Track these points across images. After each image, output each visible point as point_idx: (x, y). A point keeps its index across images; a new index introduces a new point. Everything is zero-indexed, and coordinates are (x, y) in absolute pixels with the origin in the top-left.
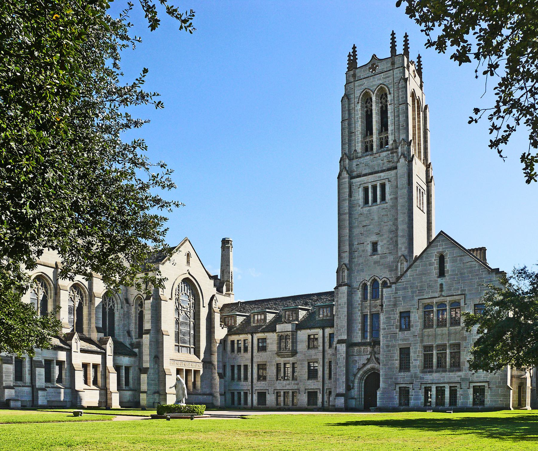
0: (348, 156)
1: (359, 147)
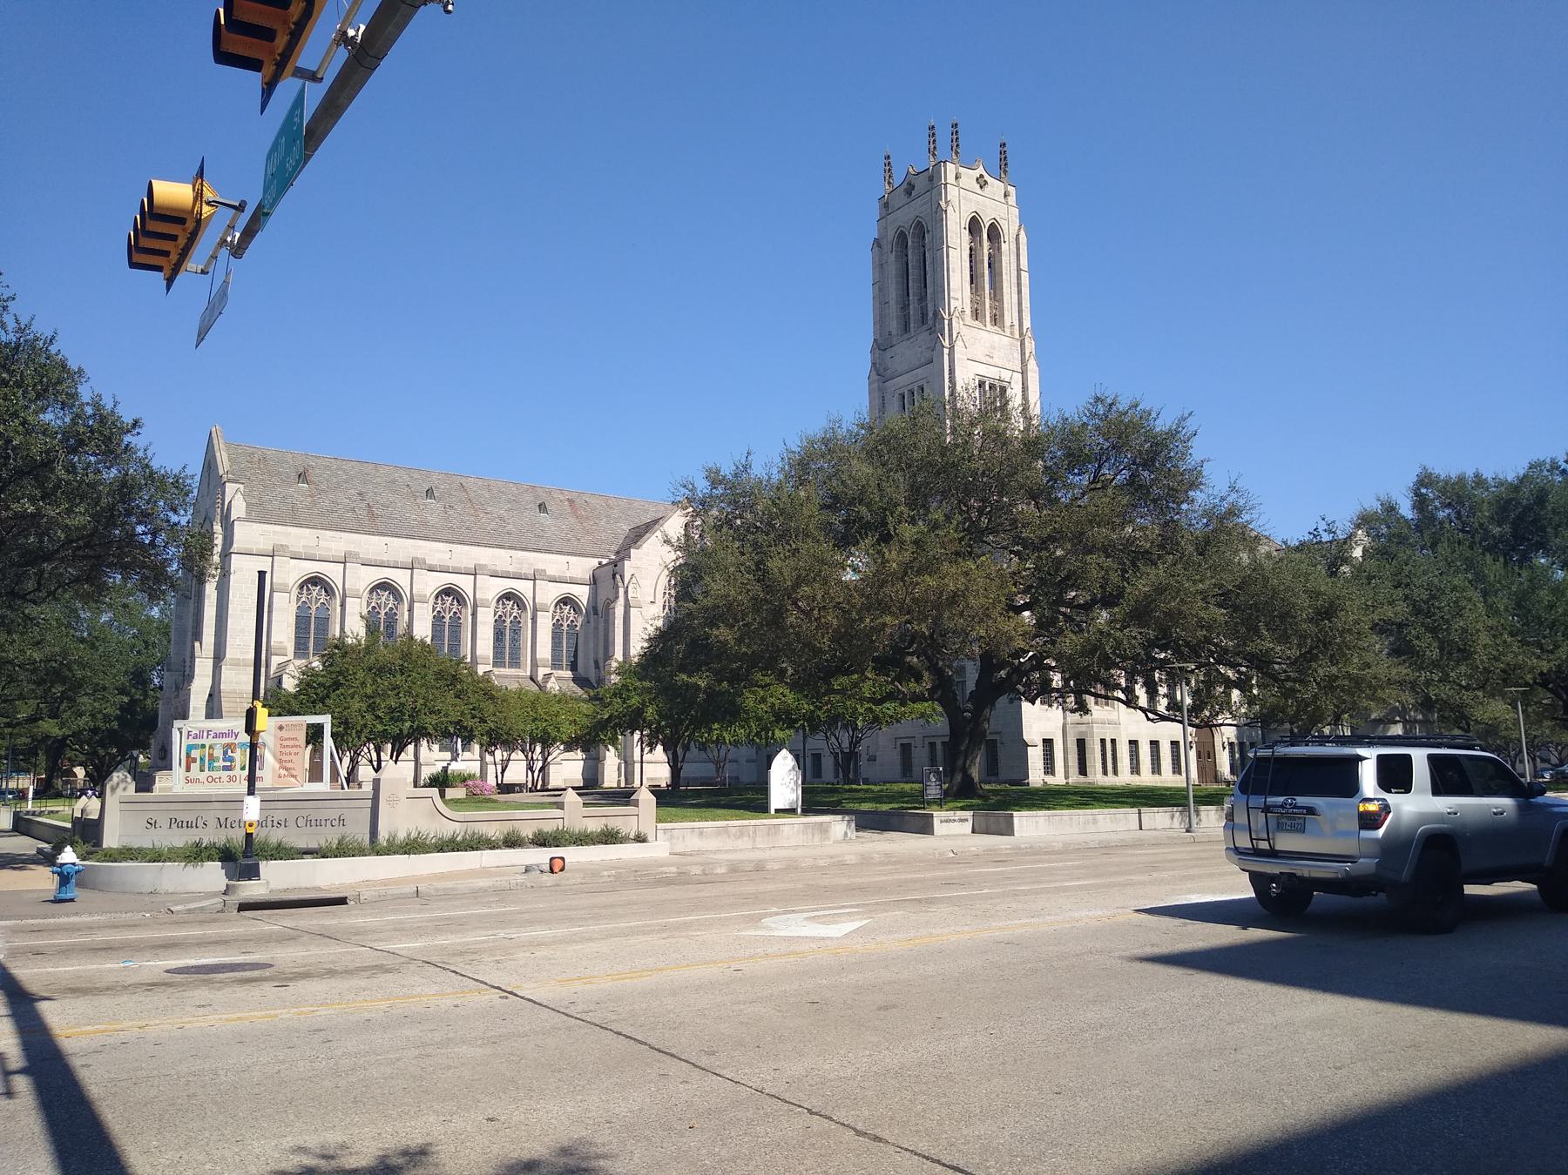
0: (882, 346)
1: (894, 325)
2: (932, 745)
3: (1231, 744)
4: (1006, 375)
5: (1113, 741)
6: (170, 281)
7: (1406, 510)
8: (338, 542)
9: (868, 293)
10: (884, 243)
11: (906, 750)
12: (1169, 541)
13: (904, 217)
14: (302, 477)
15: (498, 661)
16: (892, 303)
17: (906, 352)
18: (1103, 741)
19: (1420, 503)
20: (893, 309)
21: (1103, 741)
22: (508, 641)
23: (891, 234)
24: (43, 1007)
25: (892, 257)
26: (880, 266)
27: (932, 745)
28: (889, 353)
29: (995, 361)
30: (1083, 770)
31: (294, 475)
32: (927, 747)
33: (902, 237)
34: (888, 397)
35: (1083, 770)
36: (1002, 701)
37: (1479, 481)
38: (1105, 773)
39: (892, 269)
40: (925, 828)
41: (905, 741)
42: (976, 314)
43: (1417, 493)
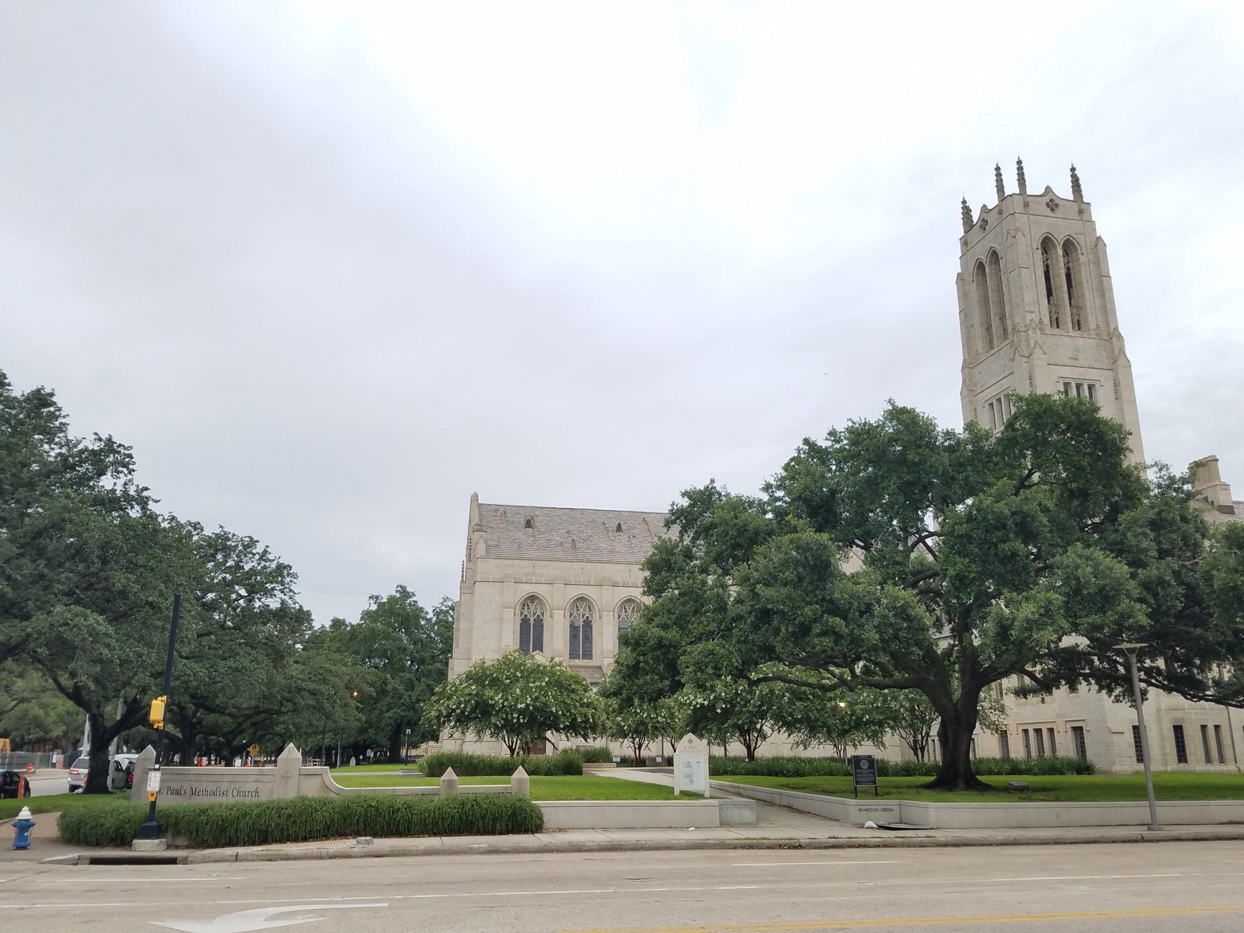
0: (969, 366)
1: (980, 345)
2: (1026, 731)
4: (1092, 375)
5: (1051, 730)
6: (967, 211)
8: (594, 570)
9: (1113, 272)
13: (982, 254)
14: (529, 524)
15: (574, 655)
16: (977, 325)
18: (1204, 727)
20: (978, 332)
22: (581, 637)
25: (973, 287)
28: (977, 370)
29: (1082, 362)
30: (1182, 756)
31: (523, 522)
33: (981, 266)
34: (979, 408)
35: (1182, 756)
38: (1208, 760)
39: (975, 296)
40: (229, 763)
42: (1056, 323)
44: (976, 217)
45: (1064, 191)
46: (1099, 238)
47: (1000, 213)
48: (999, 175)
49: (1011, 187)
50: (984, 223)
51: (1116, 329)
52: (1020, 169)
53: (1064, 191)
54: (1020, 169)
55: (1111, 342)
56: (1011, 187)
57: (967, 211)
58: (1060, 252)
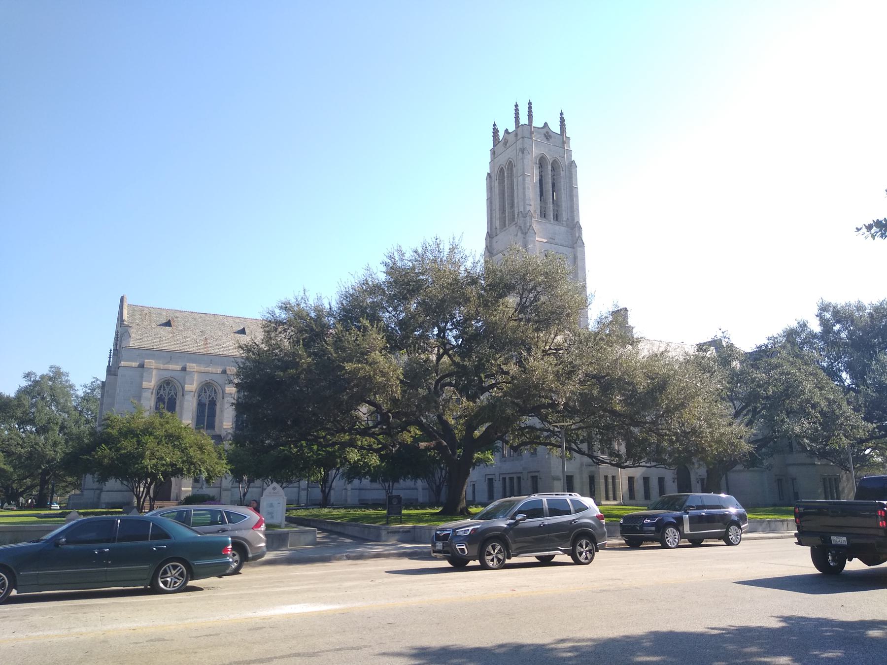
0: (490, 236)
1: (497, 223)
2: (504, 479)
3: (702, 480)
7: (816, 327)
10: (492, 175)
11: (491, 481)
12: (346, 372)
13: (502, 160)
14: (168, 324)
17: (505, 238)
18: (606, 477)
19: (824, 323)
20: (497, 214)
21: (606, 477)
23: (496, 169)
24: (811, 569)
25: (497, 183)
26: (490, 189)
27: (504, 479)
32: (530, 480)
36: (760, 437)
37: (860, 308)
39: (496, 190)
41: (490, 477)
42: (544, 215)
43: (819, 316)
44: (501, 135)
45: (555, 128)
46: (573, 162)
47: (516, 135)
48: (517, 110)
49: (524, 120)
50: (506, 142)
51: (578, 222)
52: (530, 108)
53: (555, 128)
54: (530, 108)
55: (574, 228)
56: (524, 120)
57: (496, 131)
58: (550, 168)
